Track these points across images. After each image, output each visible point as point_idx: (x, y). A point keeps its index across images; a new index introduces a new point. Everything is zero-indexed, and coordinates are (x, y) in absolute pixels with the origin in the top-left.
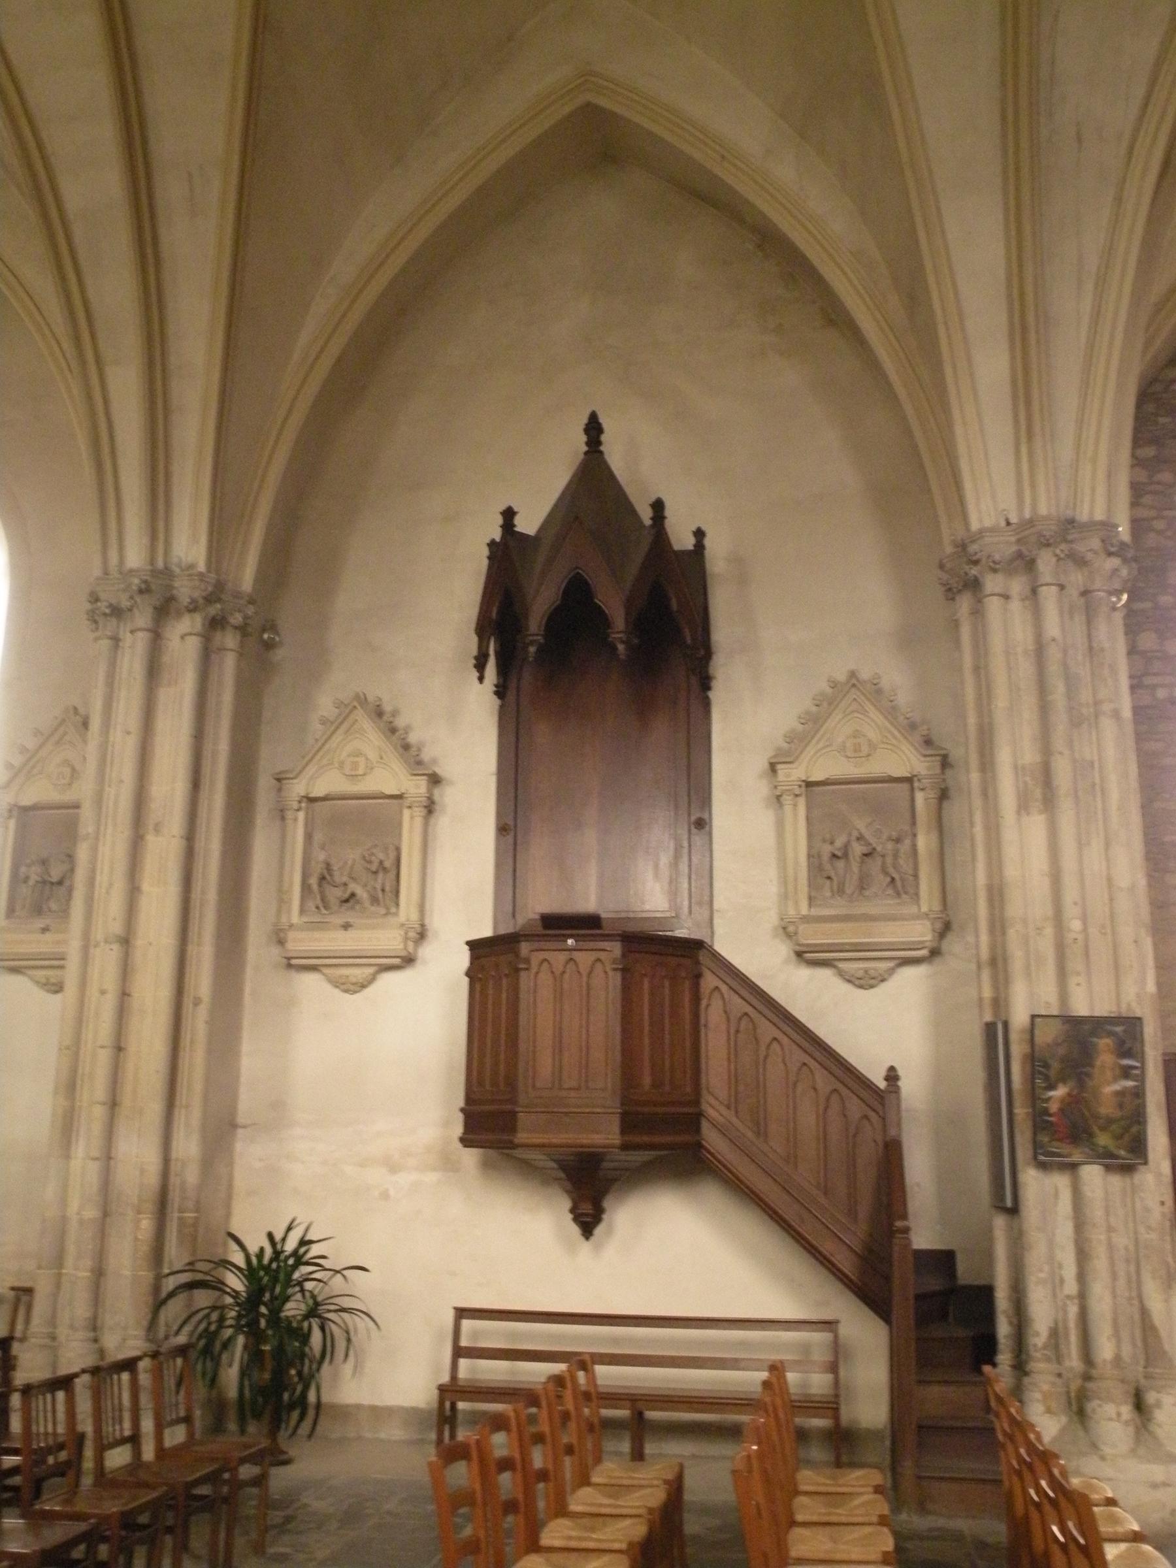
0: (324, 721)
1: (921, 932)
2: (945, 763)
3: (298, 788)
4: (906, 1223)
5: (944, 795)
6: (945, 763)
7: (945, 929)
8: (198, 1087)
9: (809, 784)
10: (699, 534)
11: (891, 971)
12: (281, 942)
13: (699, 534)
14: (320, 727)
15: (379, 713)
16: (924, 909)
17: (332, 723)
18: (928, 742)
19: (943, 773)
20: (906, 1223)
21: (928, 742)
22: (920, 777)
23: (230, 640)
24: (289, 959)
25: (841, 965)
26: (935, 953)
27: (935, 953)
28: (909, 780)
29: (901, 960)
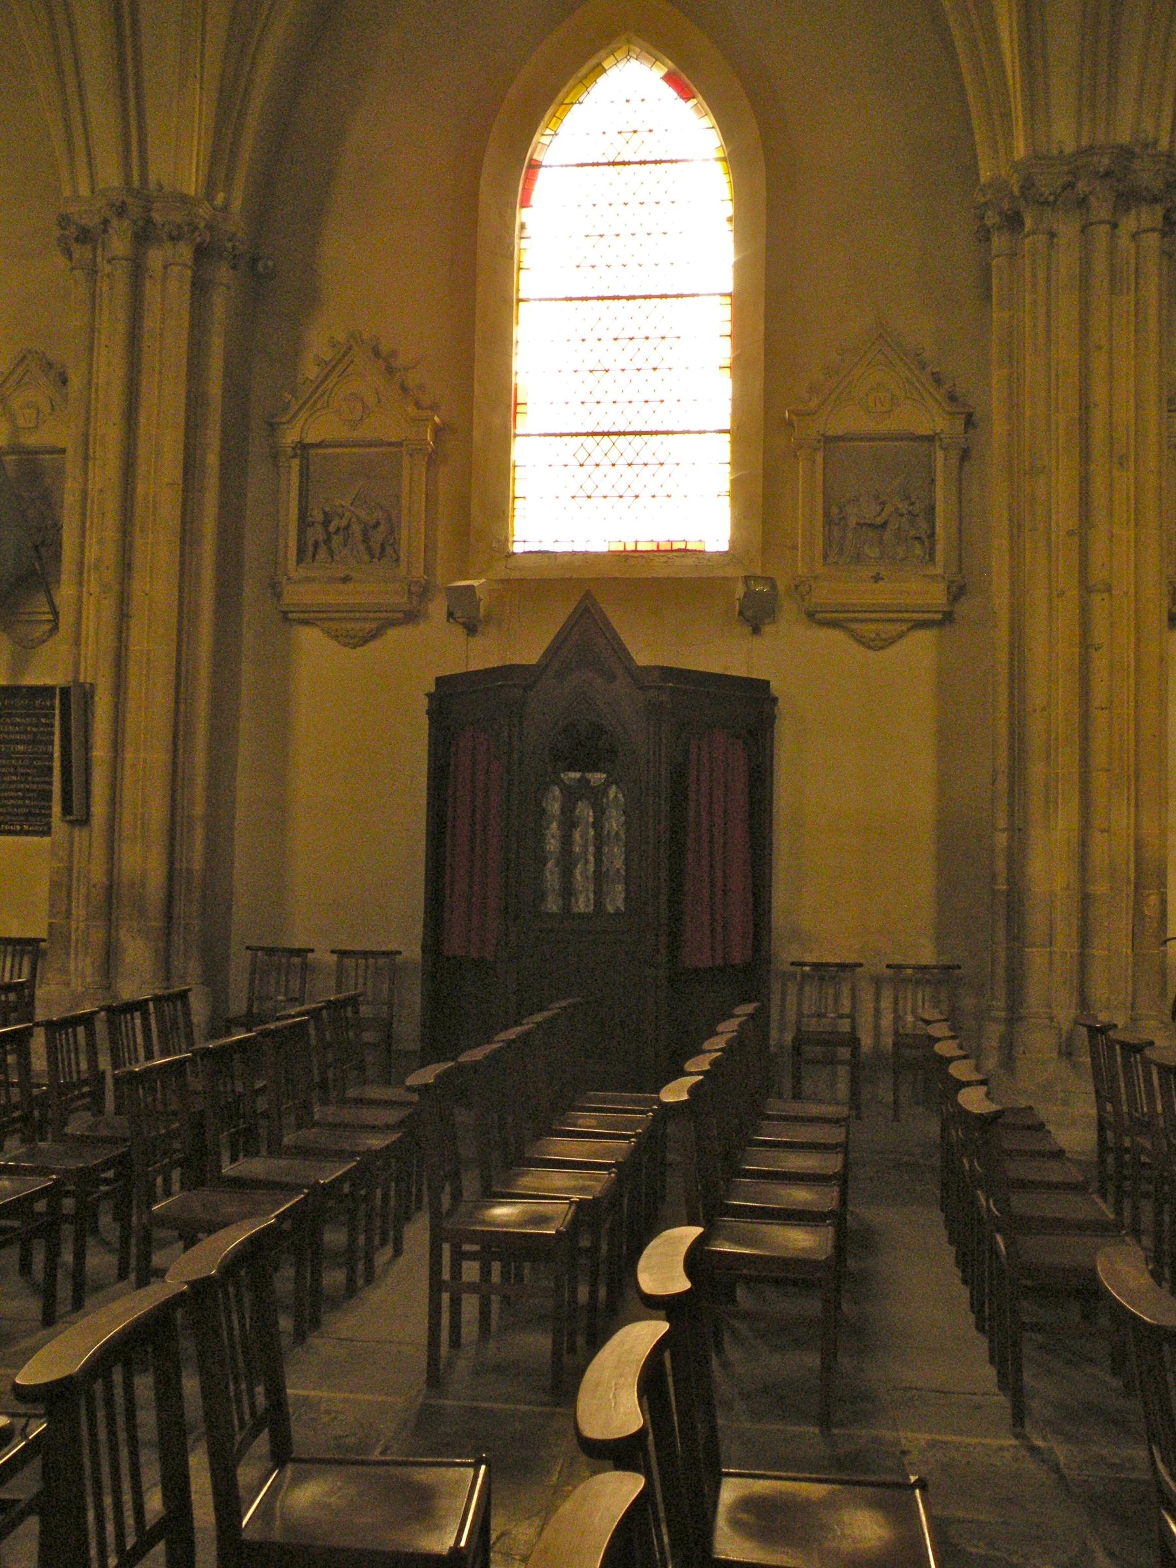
0: (319, 362)
1: (937, 595)
2: (970, 422)
3: (290, 436)
4: (264, 1152)
5: (965, 455)
6: (970, 422)
7: (958, 592)
8: (200, 780)
9: (828, 439)
10: (333, 952)
11: (901, 635)
12: (278, 596)
13: (333, 952)
14: (316, 369)
15: (377, 353)
16: (939, 570)
17: (327, 364)
18: (952, 398)
19: (966, 432)
20: (264, 1152)
21: (952, 398)
22: (943, 436)
23: (223, 273)
24: (285, 613)
25: (853, 626)
26: (948, 618)
27: (948, 618)
28: (930, 439)
29: (912, 623)
